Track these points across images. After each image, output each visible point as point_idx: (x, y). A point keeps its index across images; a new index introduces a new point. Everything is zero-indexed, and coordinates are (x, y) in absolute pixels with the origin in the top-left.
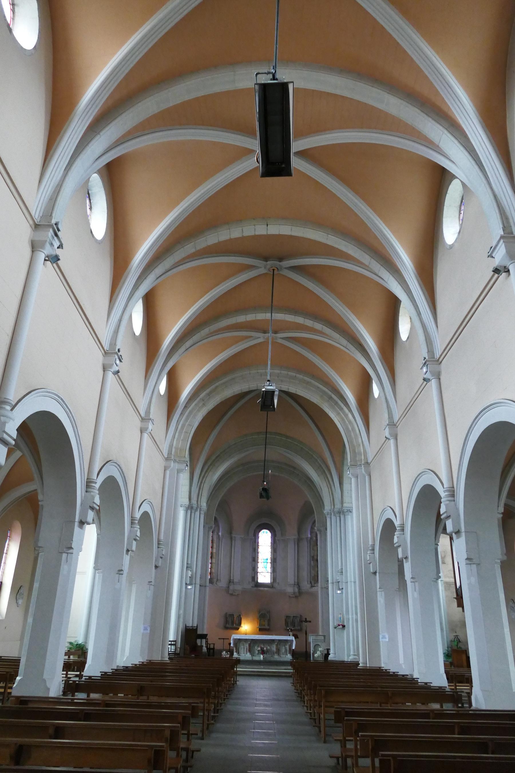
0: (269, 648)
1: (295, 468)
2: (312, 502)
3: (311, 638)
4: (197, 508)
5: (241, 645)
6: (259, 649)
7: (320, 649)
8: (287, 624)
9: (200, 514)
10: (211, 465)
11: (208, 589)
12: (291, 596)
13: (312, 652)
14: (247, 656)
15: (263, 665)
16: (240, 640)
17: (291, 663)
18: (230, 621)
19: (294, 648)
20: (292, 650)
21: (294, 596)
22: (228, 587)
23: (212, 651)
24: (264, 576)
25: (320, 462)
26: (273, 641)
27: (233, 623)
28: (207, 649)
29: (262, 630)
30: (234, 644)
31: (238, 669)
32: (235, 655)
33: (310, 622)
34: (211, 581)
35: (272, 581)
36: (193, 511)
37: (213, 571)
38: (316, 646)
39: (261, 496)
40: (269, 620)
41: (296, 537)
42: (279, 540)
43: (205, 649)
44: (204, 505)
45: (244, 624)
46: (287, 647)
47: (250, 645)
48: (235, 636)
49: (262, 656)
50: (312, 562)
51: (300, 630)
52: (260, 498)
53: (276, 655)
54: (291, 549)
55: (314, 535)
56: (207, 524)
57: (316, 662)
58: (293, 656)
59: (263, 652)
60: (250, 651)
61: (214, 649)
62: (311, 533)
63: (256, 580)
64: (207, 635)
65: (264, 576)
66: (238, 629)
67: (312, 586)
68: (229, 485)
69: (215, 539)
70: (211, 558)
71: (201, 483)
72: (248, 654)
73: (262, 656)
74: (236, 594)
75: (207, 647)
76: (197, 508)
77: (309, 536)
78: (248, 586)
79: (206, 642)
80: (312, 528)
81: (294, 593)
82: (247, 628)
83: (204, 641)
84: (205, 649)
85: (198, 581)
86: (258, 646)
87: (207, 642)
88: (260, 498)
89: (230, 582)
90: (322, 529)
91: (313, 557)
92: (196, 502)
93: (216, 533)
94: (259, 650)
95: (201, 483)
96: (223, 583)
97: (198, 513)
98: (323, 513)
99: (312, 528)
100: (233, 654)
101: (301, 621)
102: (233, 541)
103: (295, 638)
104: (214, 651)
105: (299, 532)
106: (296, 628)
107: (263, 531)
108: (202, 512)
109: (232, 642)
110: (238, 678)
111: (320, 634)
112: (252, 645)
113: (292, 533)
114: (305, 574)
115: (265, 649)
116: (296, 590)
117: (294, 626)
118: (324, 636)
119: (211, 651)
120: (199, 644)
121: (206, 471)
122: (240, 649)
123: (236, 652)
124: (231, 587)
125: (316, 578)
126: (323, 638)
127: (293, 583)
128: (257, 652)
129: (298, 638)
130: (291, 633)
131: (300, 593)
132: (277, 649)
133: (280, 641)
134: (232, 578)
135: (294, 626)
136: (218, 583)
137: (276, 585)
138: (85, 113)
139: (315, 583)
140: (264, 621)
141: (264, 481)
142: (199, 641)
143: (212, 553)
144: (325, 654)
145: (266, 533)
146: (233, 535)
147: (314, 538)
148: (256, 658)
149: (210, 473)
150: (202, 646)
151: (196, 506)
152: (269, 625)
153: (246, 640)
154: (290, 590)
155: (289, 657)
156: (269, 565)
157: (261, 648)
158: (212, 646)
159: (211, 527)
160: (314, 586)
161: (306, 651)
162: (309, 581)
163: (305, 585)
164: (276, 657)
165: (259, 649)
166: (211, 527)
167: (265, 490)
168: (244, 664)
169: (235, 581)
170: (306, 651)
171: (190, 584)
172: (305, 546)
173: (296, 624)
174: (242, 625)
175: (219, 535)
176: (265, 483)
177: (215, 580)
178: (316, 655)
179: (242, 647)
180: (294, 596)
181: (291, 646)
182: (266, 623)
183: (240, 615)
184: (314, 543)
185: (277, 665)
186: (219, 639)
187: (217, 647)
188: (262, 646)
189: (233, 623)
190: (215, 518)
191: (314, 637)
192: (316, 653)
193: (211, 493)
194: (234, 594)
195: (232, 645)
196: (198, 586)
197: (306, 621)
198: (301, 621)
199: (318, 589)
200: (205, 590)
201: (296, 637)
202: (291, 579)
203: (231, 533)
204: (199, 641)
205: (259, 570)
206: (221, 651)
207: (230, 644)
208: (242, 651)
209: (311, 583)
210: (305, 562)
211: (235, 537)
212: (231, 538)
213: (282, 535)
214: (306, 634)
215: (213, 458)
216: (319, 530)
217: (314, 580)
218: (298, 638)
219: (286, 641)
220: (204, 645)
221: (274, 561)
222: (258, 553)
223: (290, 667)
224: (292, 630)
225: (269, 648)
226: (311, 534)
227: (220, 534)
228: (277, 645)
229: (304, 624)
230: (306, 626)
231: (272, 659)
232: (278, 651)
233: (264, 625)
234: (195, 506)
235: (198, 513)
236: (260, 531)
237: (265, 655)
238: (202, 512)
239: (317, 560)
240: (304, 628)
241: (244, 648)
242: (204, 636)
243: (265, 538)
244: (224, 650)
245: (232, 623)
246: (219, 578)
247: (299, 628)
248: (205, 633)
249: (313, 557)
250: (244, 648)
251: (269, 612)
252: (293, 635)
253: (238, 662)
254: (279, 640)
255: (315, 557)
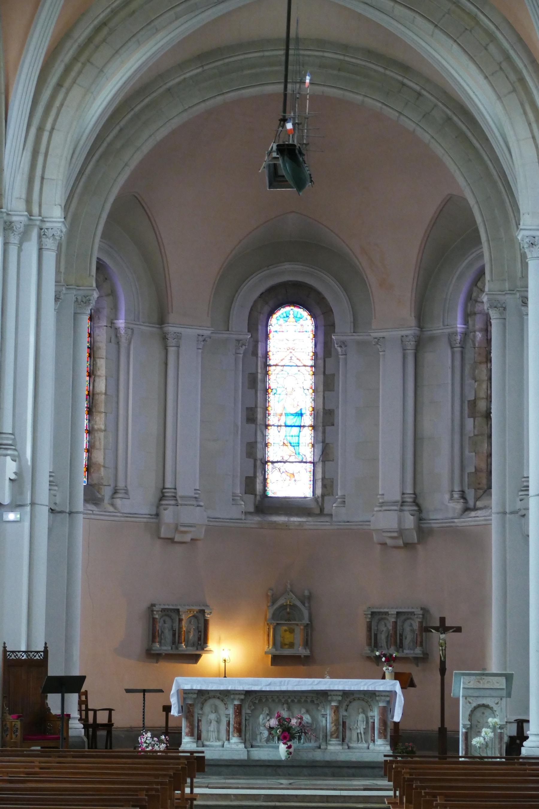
0: (307, 718)
1: (405, 68)
2: (472, 202)
3: (460, 686)
4: (28, 228)
5: (207, 708)
6: (273, 722)
7: (491, 720)
8: (373, 641)
9: (40, 250)
10: (75, 59)
11: (80, 521)
12: (389, 542)
13: (462, 730)
14: (235, 748)
15: (289, 776)
16: (203, 695)
17: (385, 769)
18: (168, 635)
19: (397, 718)
20: (390, 727)
21: (400, 543)
22: (157, 515)
23: (102, 733)
24: (290, 478)
25: (506, 45)
26: (323, 695)
27: (176, 639)
28: (86, 727)
29: (282, 661)
30: (181, 709)
31: (196, 791)
32: (188, 744)
33: (458, 630)
34: (92, 495)
35: (319, 492)
36: (14, 239)
37: (99, 457)
38: (480, 710)
39: (275, 178)
40: (309, 628)
41: (410, 331)
42: (343, 344)
43: (76, 727)
44: (55, 215)
45: (219, 641)
46: (375, 714)
47: (238, 710)
48: (185, 681)
49: (282, 747)
50: (469, 423)
51: (423, 659)
52: (271, 186)
53: (334, 741)
54: (391, 379)
55: (479, 324)
56: (68, 286)
57: (478, 762)
58: (394, 743)
59: (287, 734)
60: (239, 731)
61: (109, 726)
62: (467, 316)
63: (259, 487)
64: (82, 679)
65: (290, 478)
66: (196, 658)
67: (467, 509)
68: (148, 140)
69: (102, 336)
70: (90, 411)
71: (40, 130)
72: (234, 740)
73: (282, 747)
74: (187, 538)
75: (84, 720)
76: (28, 228)
77: (460, 327)
78: (232, 509)
79: (80, 703)
80: (471, 299)
81: (401, 532)
82: (229, 655)
83: (73, 699)
84: (76, 727)
85: (44, 496)
86: (270, 715)
87: (83, 703)
88: (271, 186)
89: (163, 496)
90: (511, 301)
91: (473, 404)
92: (21, 206)
93: (104, 322)
94: (271, 728)
95: (40, 130)
96: (138, 502)
97: (31, 248)
98: (512, 240)
99: (471, 299)
100: (180, 744)
101: (426, 629)
102: (172, 350)
103: (403, 687)
104: (109, 733)
105: (422, 316)
106: (407, 652)
107: (283, 311)
108: (50, 244)
109: (174, 701)
110: (60, 695)
111: (494, 670)
112: (246, 710)
113: (392, 316)
114: (441, 465)
115: (294, 721)
116: (410, 521)
117: (400, 646)
118: (509, 678)
119: (101, 733)
120: (56, 710)
121: (59, 85)
122: (204, 727)
123: (191, 734)
124: (168, 515)
125: (484, 475)
126: (502, 683)
127: (398, 497)
128: (266, 734)
129: (412, 684)
130: (388, 670)
131: (424, 532)
132: (336, 722)
133: (347, 696)
134: (168, 485)
135: (400, 646)
136: (118, 502)
137: (332, 506)
138: (24, 94)
139: (477, 499)
140: (292, 631)
141: (284, 120)
142: (53, 701)
143: (91, 396)
144: (511, 738)
145: (297, 319)
146: (171, 329)
147: (479, 335)
148: (262, 754)
149: (76, 93)
150: (65, 718)
151: (24, 219)
152: (307, 643)
153: (224, 695)
154: (386, 521)
155: (380, 749)
156: (307, 436)
157: (281, 720)
158: (102, 718)
159: (86, 301)
160: (475, 509)
161: (442, 730)
162: (457, 488)
163: (443, 506)
164: (335, 750)
165: (273, 722)
166: (86, 301)
167: (289, 151)
168: (219, 774)
169: (180, 493)
170: (442, 730)
171: (16, 506)
172: (441, 363)
173: (407, 642)
174: (212, 645)
175: (117, 329)
176: (289, 126)
177: (107, 492)
178: (476, 741)
179: (213, 716)
180: (400, 543)
181: (387, 711)
182: (298, 637)
183: (203, 612)
184: (476, 355)
185: (334, 776)
186: (128, 691)
187: (120, 721)
188: (285, 714)
189: (176, 639)
190: (101, 266)
191: (472, 682)
192: (478, 734)
193: (81, 172)
194: (178, 538)
195: (174, 712)
196: (43, 513)
197: (443, 628)
198: (426, 629)
199: (491, 517)
200: (71, 535)
201: (407, 682)
202: (390, 483)
203: (162, 321)
204: (53, 701)
205: (273, 453)
206: (133, 735)
207: (167, 709)
208: (209, 729)
209: (463, 496)
210: (442, 421)
211: (178, 336)
212: (164, 338)
213: (355, 327)
214: (443, 670)
215: (82, 34)
216: (493, 306)
217: (476, 484)
218: (412, 684)
219: (371, 696)
220: (75, 714)
221: (325, 420)
222: (266, 391)
223: (385, 782)
224: (390, 660)
225: (307, 718)
226: (466, 322)
227: (121, 323)
228: (337, 710)
229: (438, 637)
230: (443, 645)
231: (318, 756)
232: (342, 731)
233: (291, 645)
234: (19, 219)
235: (31, 248)
236: (271, 313)
237: (294, 744)
238: (50, 244)
239: (488, 415)
240: (436, 654)
241: (218, 722)
242: (73, 684)
243: (291, 334)
244: (145, 729)
245: (175, 636)
246: (121, 484)
247: (418, 651)
248: (76, 672)
249: (473, 404)
250: (218, 722)
251: (308, 599)
252: (397, 676)
253: (197, 765)
254: (346, 694)
255: (482, 405)
